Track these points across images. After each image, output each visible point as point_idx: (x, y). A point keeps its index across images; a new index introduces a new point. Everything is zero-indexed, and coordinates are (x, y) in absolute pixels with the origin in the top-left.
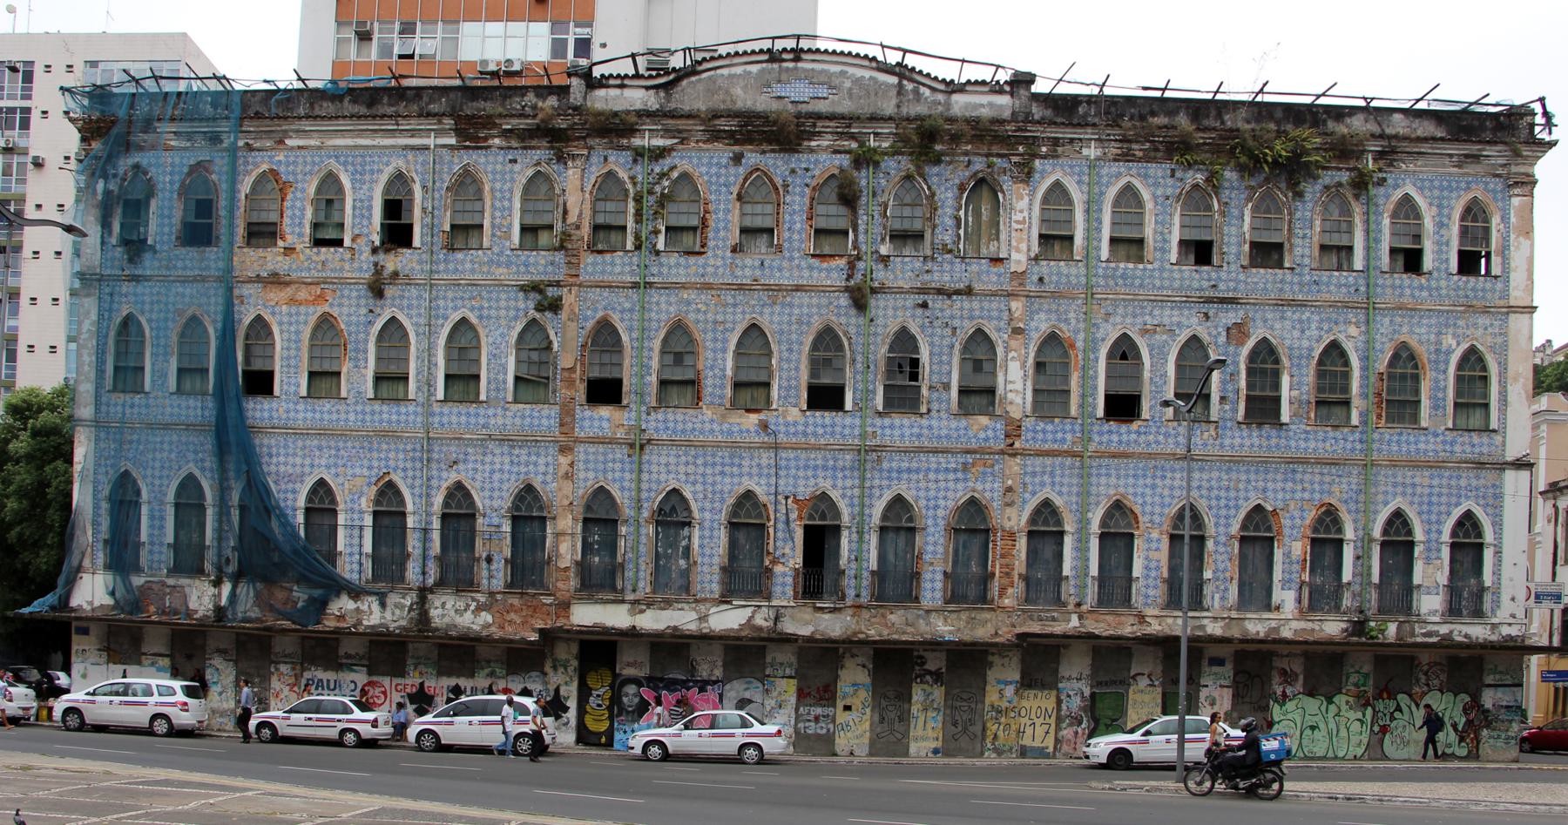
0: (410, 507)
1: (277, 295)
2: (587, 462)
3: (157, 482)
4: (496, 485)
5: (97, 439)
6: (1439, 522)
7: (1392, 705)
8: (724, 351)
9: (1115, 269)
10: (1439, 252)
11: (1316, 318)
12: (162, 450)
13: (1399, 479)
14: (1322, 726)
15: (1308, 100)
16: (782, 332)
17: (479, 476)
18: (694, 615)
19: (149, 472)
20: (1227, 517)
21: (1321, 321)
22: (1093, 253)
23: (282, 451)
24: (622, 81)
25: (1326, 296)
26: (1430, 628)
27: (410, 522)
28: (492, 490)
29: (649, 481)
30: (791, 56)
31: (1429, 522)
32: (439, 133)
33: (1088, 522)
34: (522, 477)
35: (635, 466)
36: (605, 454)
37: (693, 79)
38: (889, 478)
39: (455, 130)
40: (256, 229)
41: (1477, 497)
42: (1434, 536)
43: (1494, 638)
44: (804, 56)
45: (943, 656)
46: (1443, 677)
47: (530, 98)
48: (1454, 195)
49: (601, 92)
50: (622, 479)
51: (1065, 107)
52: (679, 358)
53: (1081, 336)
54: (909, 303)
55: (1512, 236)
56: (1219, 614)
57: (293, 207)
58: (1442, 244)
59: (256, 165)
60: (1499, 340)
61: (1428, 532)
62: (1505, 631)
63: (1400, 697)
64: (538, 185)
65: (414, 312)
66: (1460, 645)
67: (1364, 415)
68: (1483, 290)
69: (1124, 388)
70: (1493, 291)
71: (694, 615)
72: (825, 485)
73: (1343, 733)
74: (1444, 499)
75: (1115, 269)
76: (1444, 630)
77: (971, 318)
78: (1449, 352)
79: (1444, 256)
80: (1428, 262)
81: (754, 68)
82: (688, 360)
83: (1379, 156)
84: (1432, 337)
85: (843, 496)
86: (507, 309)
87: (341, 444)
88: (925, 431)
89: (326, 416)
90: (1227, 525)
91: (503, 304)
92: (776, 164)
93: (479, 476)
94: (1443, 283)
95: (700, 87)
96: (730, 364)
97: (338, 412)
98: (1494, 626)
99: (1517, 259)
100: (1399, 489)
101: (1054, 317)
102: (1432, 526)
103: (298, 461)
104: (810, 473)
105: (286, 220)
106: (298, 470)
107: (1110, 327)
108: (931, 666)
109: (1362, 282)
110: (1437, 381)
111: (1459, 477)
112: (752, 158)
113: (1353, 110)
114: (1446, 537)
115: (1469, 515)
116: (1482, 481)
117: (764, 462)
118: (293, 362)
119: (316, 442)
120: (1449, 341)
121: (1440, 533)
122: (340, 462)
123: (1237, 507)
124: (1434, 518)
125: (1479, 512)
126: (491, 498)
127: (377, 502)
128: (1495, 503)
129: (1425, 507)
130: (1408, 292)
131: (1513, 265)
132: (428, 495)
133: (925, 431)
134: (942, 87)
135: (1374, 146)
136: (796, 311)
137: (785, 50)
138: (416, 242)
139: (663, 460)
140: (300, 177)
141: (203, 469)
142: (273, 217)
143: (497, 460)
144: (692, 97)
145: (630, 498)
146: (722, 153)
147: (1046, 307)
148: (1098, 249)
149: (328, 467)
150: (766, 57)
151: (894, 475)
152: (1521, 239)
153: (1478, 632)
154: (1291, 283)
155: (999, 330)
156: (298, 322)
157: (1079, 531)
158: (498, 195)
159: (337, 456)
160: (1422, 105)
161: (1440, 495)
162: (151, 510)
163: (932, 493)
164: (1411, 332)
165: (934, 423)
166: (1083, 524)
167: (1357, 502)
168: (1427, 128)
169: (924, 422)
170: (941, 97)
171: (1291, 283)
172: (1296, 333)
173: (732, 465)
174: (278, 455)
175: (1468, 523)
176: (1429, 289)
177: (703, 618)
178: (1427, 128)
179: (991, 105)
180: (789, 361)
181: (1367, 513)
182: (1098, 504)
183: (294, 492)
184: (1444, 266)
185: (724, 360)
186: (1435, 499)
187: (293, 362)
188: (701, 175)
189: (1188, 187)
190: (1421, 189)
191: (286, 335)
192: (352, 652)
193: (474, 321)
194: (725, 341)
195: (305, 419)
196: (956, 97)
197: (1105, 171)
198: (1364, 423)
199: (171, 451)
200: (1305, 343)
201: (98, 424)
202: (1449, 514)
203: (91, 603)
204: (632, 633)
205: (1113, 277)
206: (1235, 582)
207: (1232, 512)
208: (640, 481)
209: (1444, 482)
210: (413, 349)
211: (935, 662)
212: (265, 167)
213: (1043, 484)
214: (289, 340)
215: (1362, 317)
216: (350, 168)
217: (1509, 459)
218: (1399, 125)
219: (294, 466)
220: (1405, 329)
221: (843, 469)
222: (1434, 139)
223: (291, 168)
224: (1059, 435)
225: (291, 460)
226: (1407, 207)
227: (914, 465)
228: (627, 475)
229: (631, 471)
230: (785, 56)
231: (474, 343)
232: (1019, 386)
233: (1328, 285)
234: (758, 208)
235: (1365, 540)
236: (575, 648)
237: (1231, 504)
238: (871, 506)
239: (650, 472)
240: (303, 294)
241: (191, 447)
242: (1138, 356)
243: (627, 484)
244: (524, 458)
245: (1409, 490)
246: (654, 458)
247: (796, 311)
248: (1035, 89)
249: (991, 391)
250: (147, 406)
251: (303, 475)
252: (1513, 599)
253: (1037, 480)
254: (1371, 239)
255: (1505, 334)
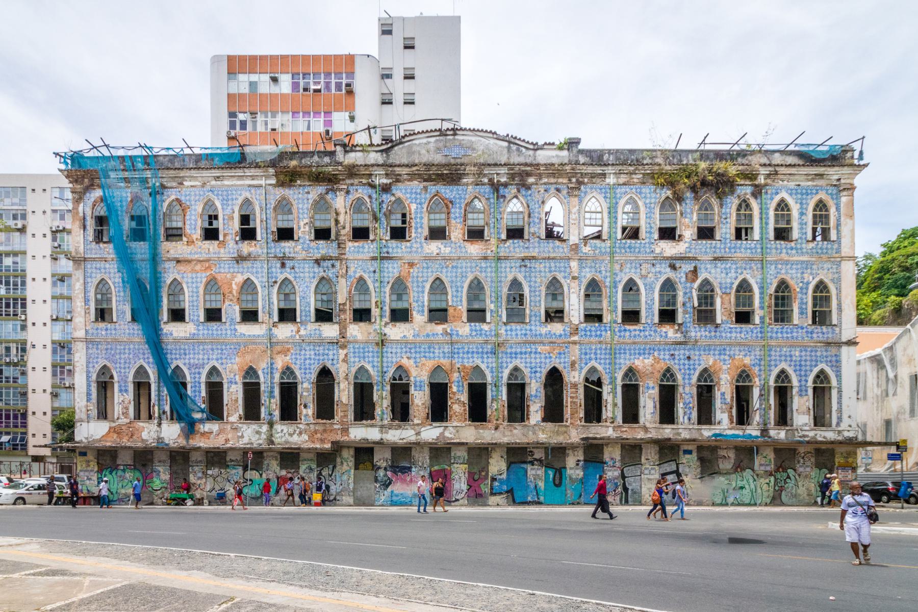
0: (262, 380)
1: (182, 267)
2: (354, 353)
3: (123, 371)
4: (307, 366)
5: (87, 348)
6: (806, 376)
7: (785, 475)
8: (423, 292)
9: (625, 244)
10: (801, 229)
11: (734, 266)
12: (125, 353)
13: (783, 353)
14: (747, 486)
15: (727, 147)
16: (452, 282)
17: (298, 362)
18: (413, 432)
19: (118, 365)
20: (689, 375)
21: (737, 268)
22: (613, 235)
23: (192, 352)
24: (364, 149)
25: (739, 255)
26: (804, 433)
27: (262, 388)
28: (306, 369)
29: (387, 362)
30: (451, 132)
31: (801, 376)
32: (267, 177)
33: (616, 378)
34: (321, 362)
35: (380, 355)
36: (363, 348)
37: (401, 146)
38: (511, 358)
39: (276, 176)
40: (170, 232)
41: (827, 361)
42: (803, 383)
43: (840, 438)
44: (458, 132)
45: (543, 451)
46: (813, 460)
47: (316, 158)
48: (809, 197)
49: (352, 155)
50: (373, 362)
51: (597, 157)
52: (400, 297)
53: (608, 280)
54: (518, 265)
55: (842, 219)
56: (685, 427)
57: (190, 219)
58: (802, 224)
59: (169, 196)
60: (836, 276)
61: (800, 381)
62: (846, 434)
63: (789, 471)
64: (321, 205)
65: (259, 275)
66: (821, 442)
67: (762, 319)
68: (827, 249)
69: (631, 307)
70: (832, 249)
71: (413, 432)
72: (478, 362)
73: (759, 491)
74: (808, 363)
75: (625, 244)
76: (811, 434)
77: (550, 272)
78: (808, 283)
79: (804, 231)
80: (795, 234)
81: (433, 140)
82: (405, 297)
83: (768, 176)
84: (799, 275)
85: (488, 367)
86: (309, 272)
87: (224, 347)
88: (528, 332)
89: (215, 332)
90: (690, 379)
91: (307, 270)
92: (447, 191)
93: (298, 362)
94: (804, 246)
95: (404, 151)
96: (426, 298)
97: (221, 330)
98: (839, 432)
99: (845, 230)
100: (783, 358)
101: (593, 270)
102: (802, 378)
103: (201, 357)
104: (470, 355)
105: (187, 227)
106: (201, 361)
107: (623, 275)
108: (537, 456)
109: (758, 246)
110: (802, 299)
111: (816, 351)
112: (433, 188)
113: (753, 153)
114: (810, 383)
115: (822, 372)
116: (829, 353)
117: (446, 350)
118: (195, 304)
119: (210, 346)
120: (807, 277)
121: (807, 381)
122: (224, 357)
123: (695, 369)
124: (803, 373)
125: (828, 370)
126: (305, 373)
127: (245, 378)
128: (837, 365)
129: (798, 368)
130: (784, 251)
131: (843, 234)
132: (272, 373)
133: (528, 332)
134: (531, 147)
135: (764, 171)
136: (460, 270)
137: (448, 129)
138: (259, 237)
139: (394, 351)
140: (193, 203)
141: (148, 363)
142: (180, 225)
143: (308, 353)
144: (399, 155)
145: (378, 371)
146: (416, 185)
147: (589, 265)
148: (616, 233)
149: (217, 360)
150: (438, 133)
151: (513, 355)
152: (848, 220)
153: (830, 435)
154: (720, 248)
155: (565, 277)
156: (197, 282)
157: (611, 383)
158: (301, 211)
159: (221, 354)
160: (792, 148)
161: (806, 361)
162: (120, 386)
163: (533, 365)
164: (787, 273)
165: (533, 328)
166: (613, 381)
167: (760, 365)
168: (791, 160)
169: (528, 327)
170: (531, 152)
171: (720, 248)
172: (723, 275)
173: (430, 352)
174: (190, 354)
175: (822, 376)
176: (796, 249)
177: (418, 434)
178: (791, 160)
179: (557, 156)
180: (457, 297)
181: (500, 368)
182: (620, 368)
183: (199, 373)
184: (804, 236)
185: (423, 297)
186: (803, 363)
187: (195, 304)
188: (407, 199)
189: (663, 198)
190: (791, 194)
191: (190, 289)
192: (233, 458)
193: (292, 279)
194: (423, 287)
195: (203, 334)
196: (539, 152)
197: (618, 191)
198: (762, 322)
199: (129, 354)
200: (729, 281)
201: (88, 341)
202: (811, 371)
203: (87, 438)
204: (380, 443)
205: (624, 248)
206: (696, 409)
207: (692, 372)
208: (382, 362)
209: (808, 353)
210: (260, 295)
211: (539, 454)
212: (173, 197)
213: (590, 359)
214: (192, 292)
215: (759, 266)
216: (221, 198)
217: (844, 339)
218: (777, 159)
219: (198, 359)
220: (783, 271)
221: (487, 353)
222: (799, 165)
223: (188, 198)
224: (599, 333)
225: (196, 356)
226: (783, 206)
227: (524, 350)
228: (376, 359)
229: (378, 357)
230: (448, 133)
231: (293, 291)
232: (577, 307)
233: (740, 248)
234: (437, 216)
235: (764, 388)
236: (352, 452)
237: (692, 367)
238: (502, 372)
239: (387, 357)
240: (198, 267)
241: (141, 351)
242: (638, 290)
243: (375, 364)
244: (321, 352)
245: (789, 359)
246: (389, 350)
247: (460, 270)
248: (581, 147)
249: (561, 311)
250: (115, 329)
251: (204, 364)
252: (850, 417)
253: (588, 357)
254: (763, 223)
255: (839, 273)
